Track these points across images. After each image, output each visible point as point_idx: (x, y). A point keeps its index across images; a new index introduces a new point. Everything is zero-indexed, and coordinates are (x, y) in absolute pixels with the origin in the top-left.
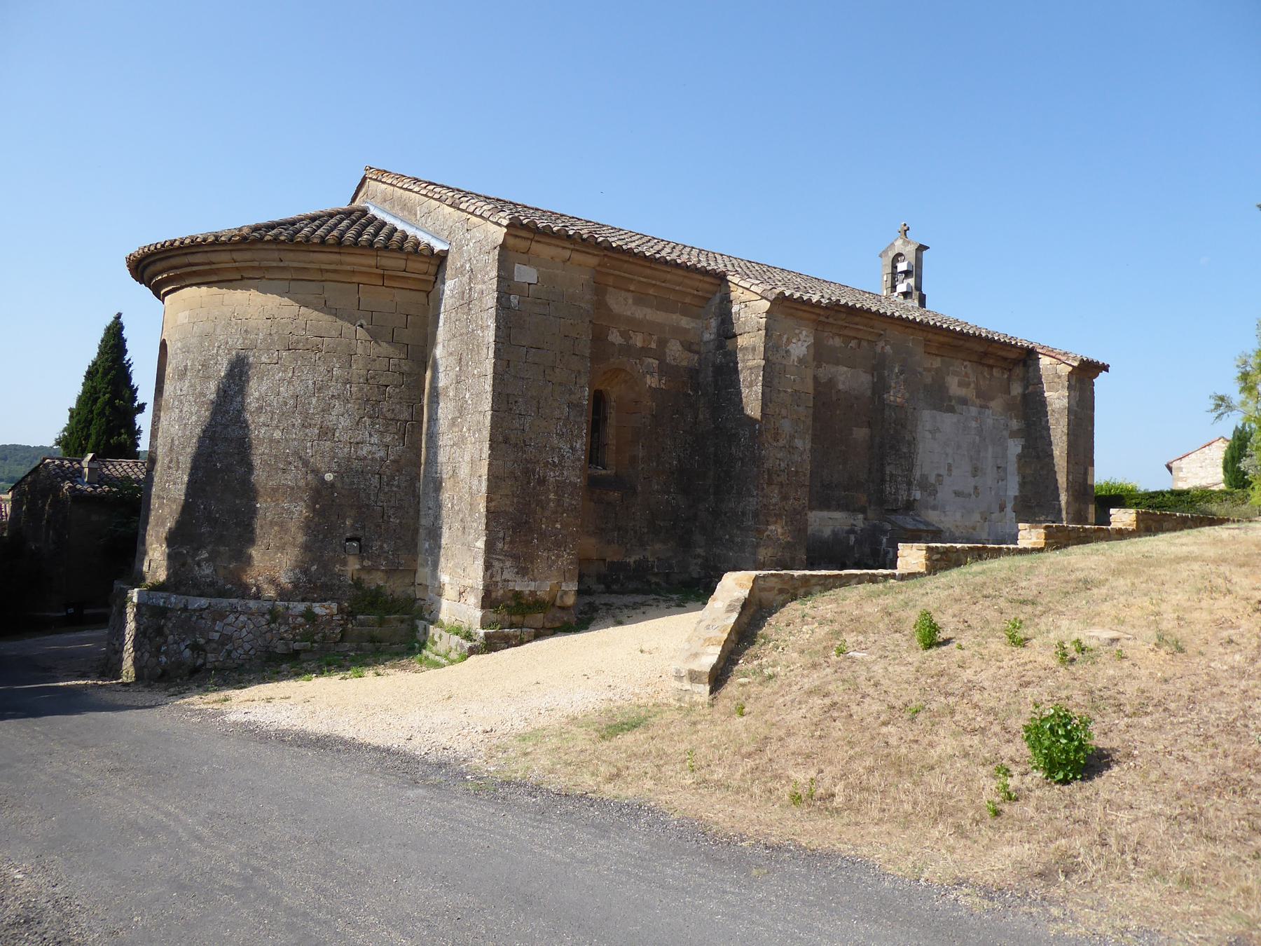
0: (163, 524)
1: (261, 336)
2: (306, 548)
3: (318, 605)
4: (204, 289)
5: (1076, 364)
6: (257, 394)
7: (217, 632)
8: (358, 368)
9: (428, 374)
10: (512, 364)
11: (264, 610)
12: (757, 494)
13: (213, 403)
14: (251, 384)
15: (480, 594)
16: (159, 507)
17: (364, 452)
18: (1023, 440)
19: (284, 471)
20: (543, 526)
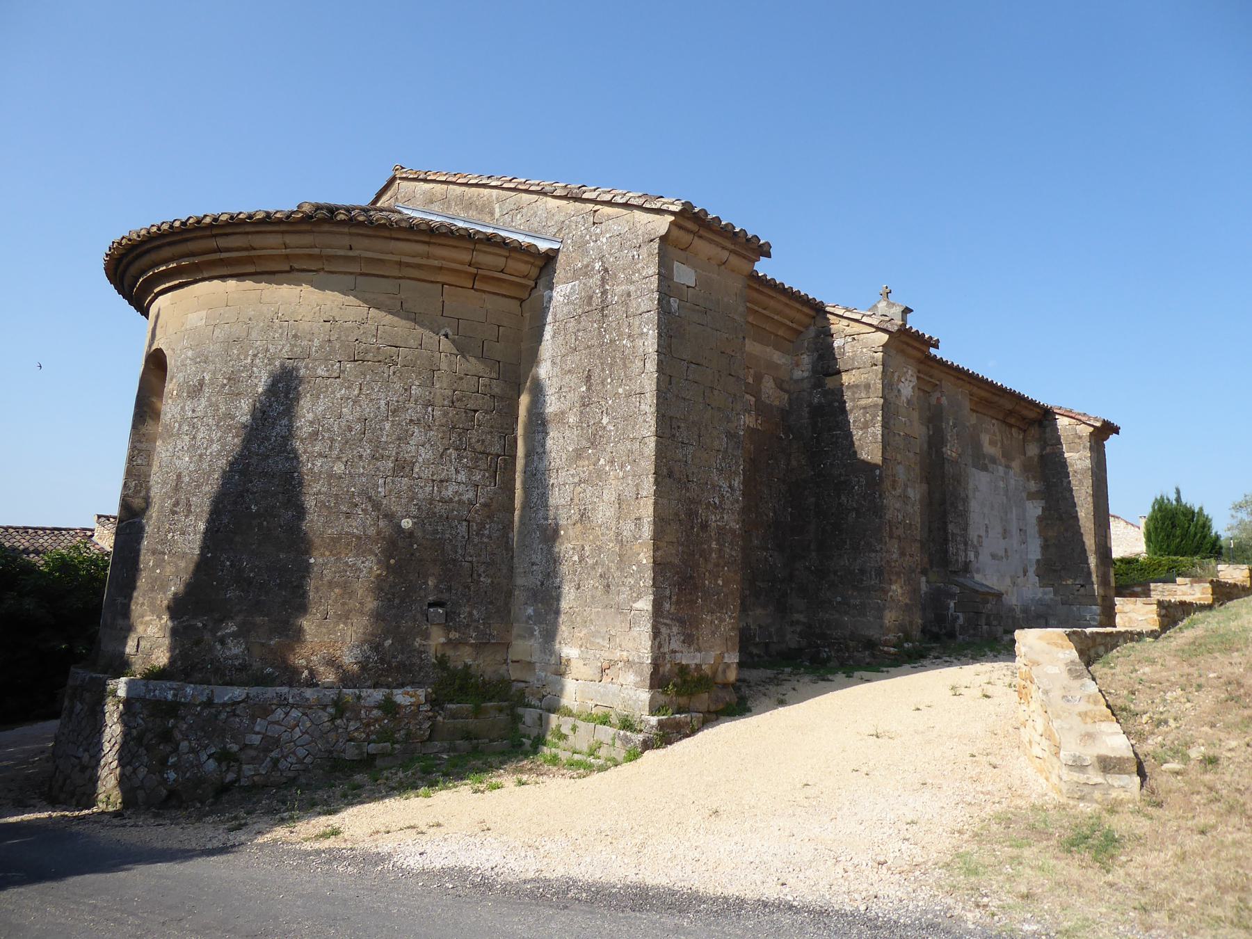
0: (164, 588)
1: (316, 343)
2: (378, 616)
3: (399, 691)
4: (232, 283)
5: (1098, 424)
6: (310, 416)
7: (258, 733)
8: (441, 387)
9: (524, 400)
10: (674, 382)
11: (327, 701)
12: (881, 549)
13: (246, 427)
14: (302, 402)
15: (648, 671)
16: (156, 566)
17: (450, 493)
18: (1043, 501)
19: (348, 515)
20: (707, 582)
